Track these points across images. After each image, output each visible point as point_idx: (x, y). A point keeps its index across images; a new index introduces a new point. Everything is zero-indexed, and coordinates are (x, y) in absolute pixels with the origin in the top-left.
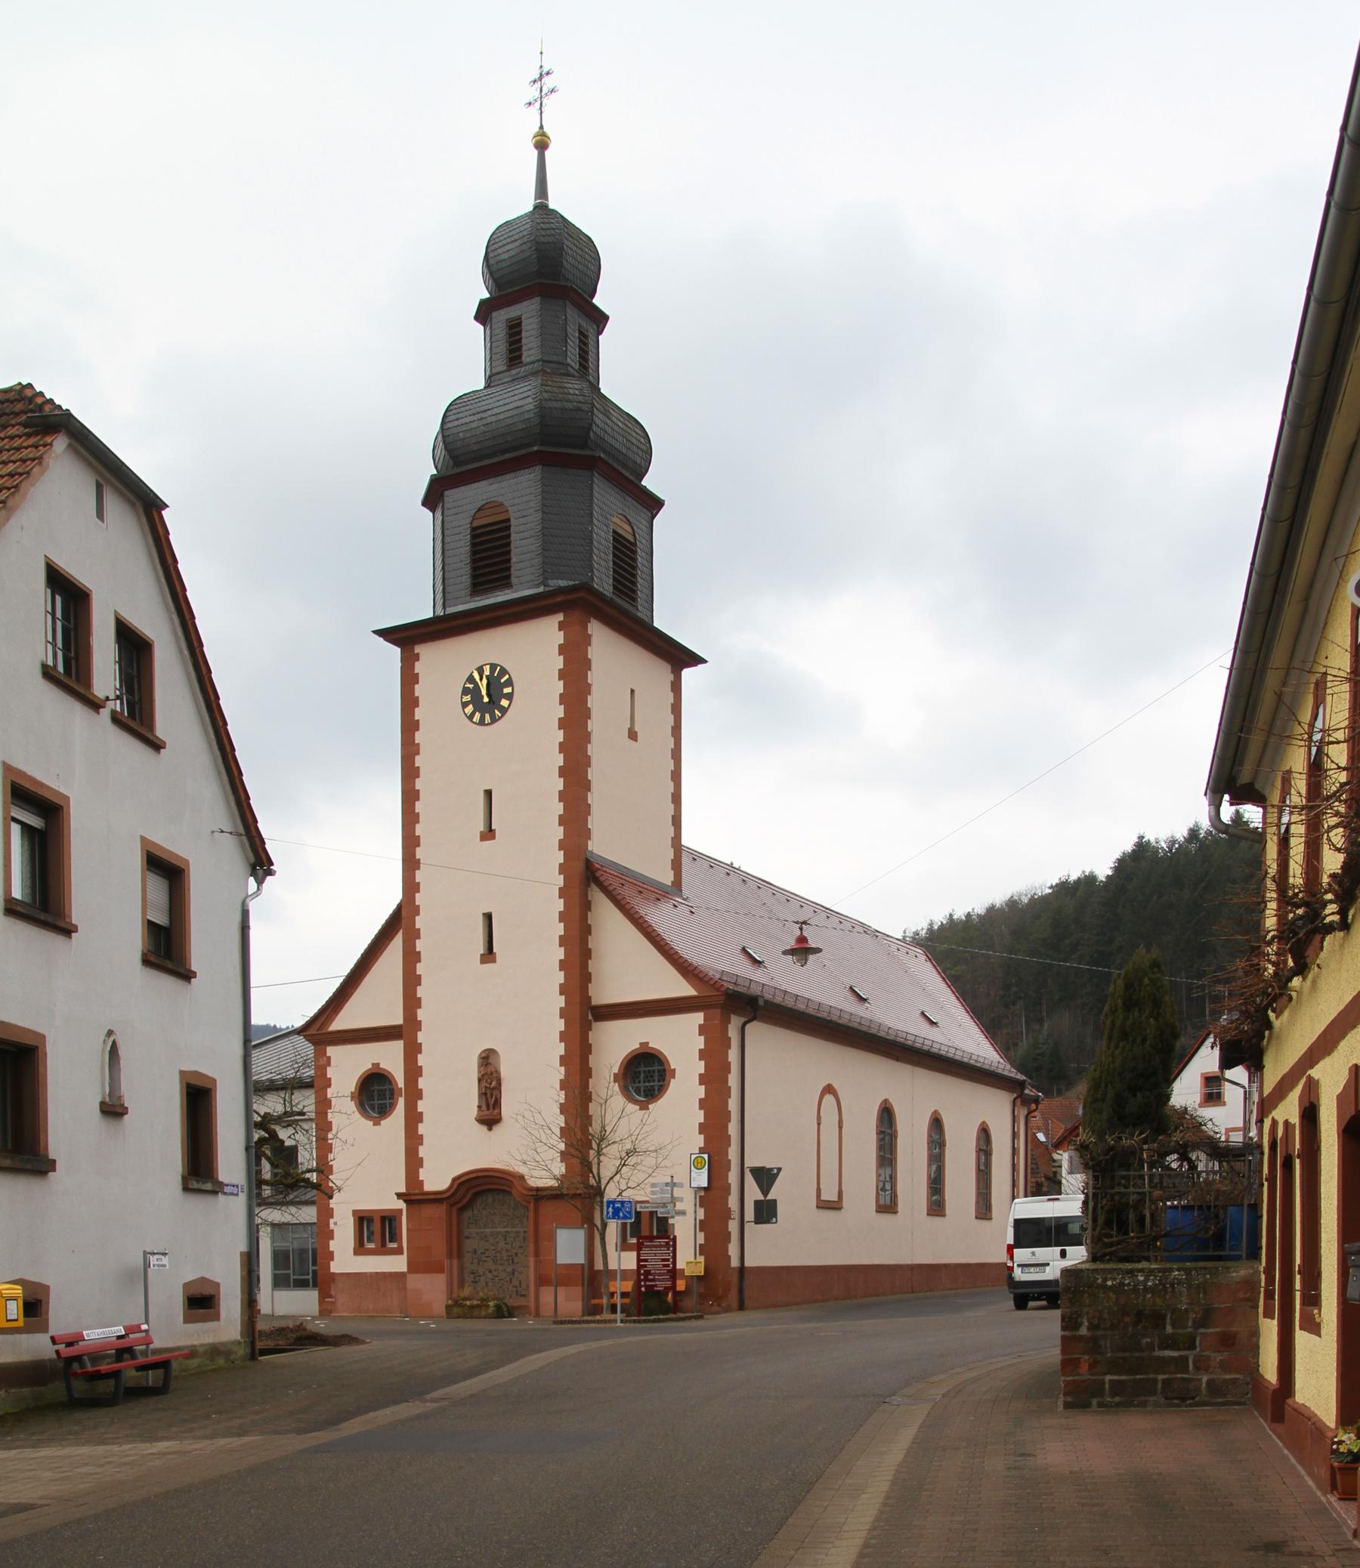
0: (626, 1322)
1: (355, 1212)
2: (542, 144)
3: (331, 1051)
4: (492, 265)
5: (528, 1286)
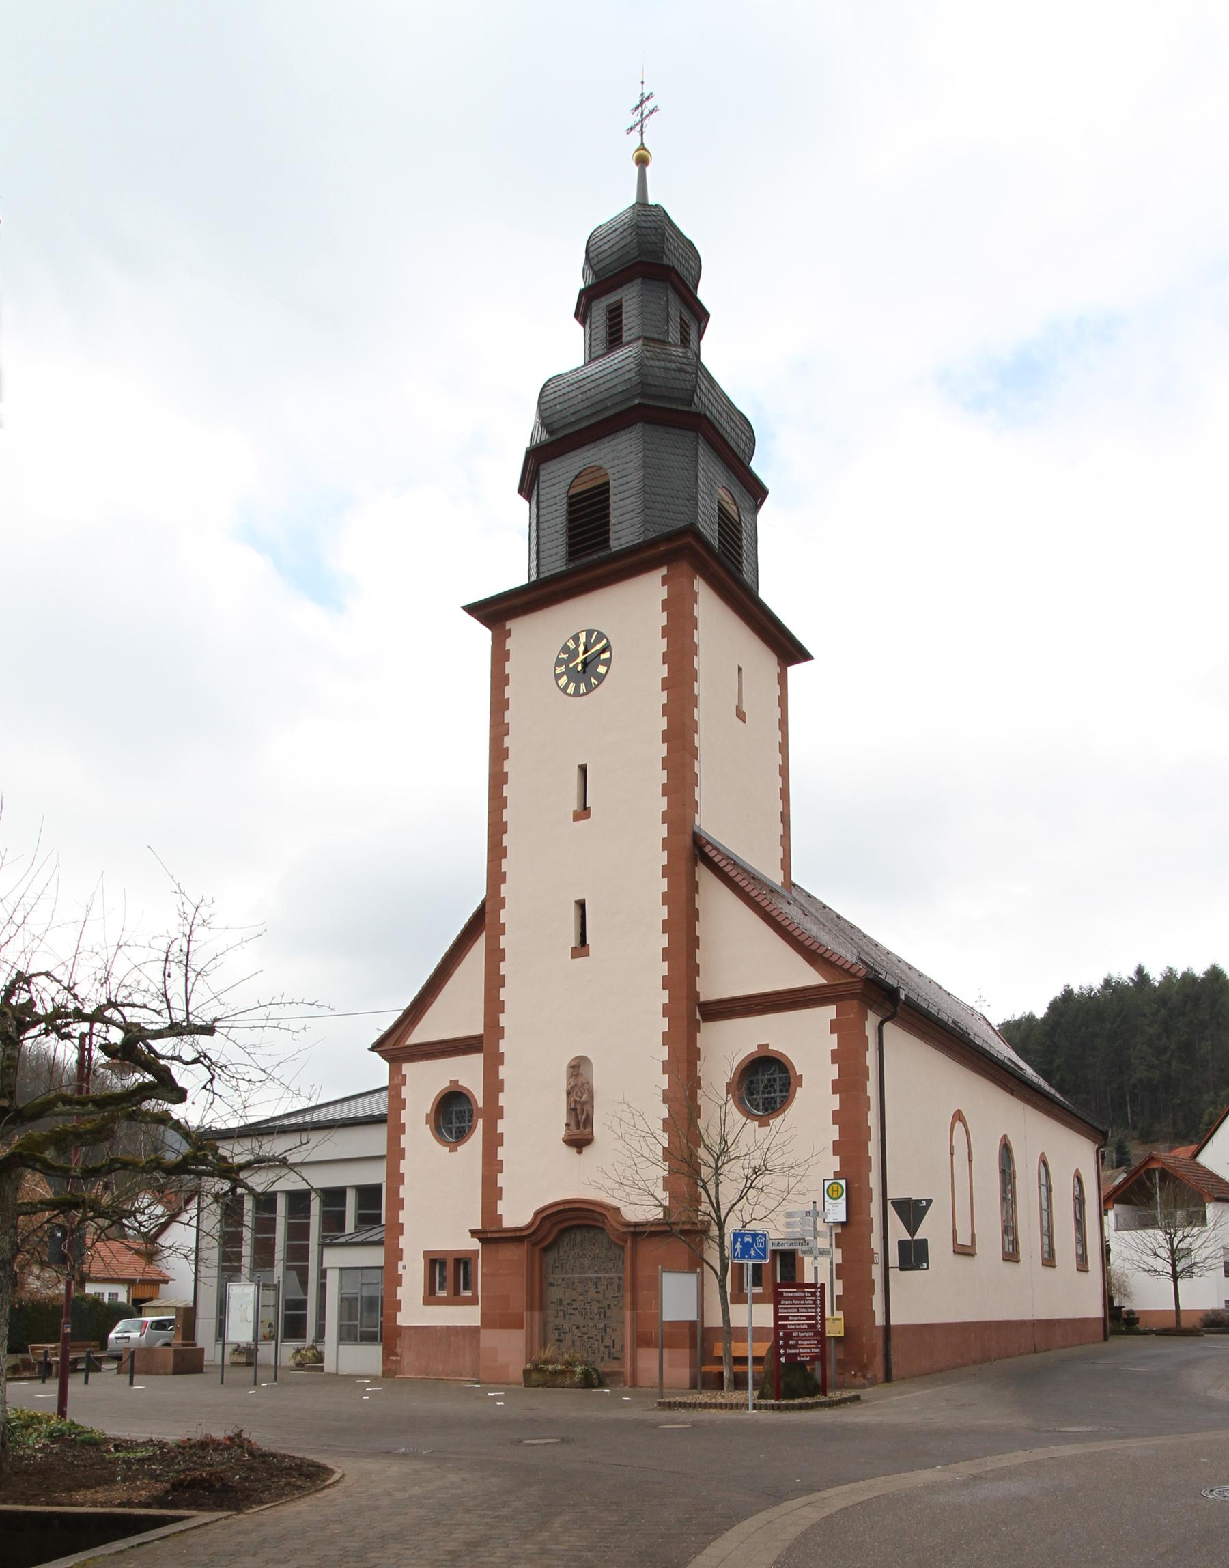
0: (760, 1409)
1: (426, 1253)
2: (642, 161)
3: (407, 1068)
4: (593, 258)
5: (623, 1347)
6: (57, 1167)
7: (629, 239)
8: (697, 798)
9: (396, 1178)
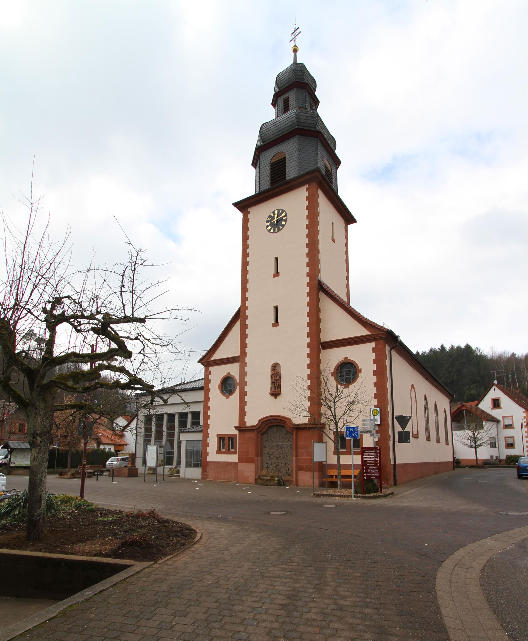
2: (295, 51)
3: (211, 369)
5: (292, 471)
6: (71, 387)
7: (292, 74)
8: (319, 268)
9: (207, 408)
